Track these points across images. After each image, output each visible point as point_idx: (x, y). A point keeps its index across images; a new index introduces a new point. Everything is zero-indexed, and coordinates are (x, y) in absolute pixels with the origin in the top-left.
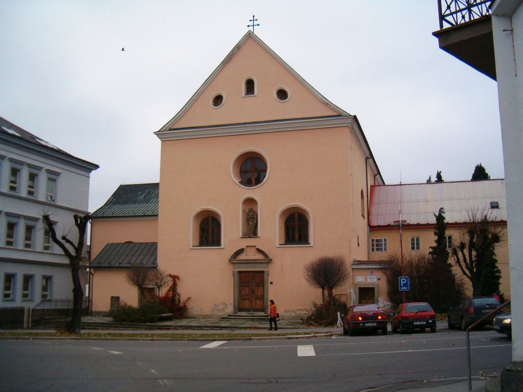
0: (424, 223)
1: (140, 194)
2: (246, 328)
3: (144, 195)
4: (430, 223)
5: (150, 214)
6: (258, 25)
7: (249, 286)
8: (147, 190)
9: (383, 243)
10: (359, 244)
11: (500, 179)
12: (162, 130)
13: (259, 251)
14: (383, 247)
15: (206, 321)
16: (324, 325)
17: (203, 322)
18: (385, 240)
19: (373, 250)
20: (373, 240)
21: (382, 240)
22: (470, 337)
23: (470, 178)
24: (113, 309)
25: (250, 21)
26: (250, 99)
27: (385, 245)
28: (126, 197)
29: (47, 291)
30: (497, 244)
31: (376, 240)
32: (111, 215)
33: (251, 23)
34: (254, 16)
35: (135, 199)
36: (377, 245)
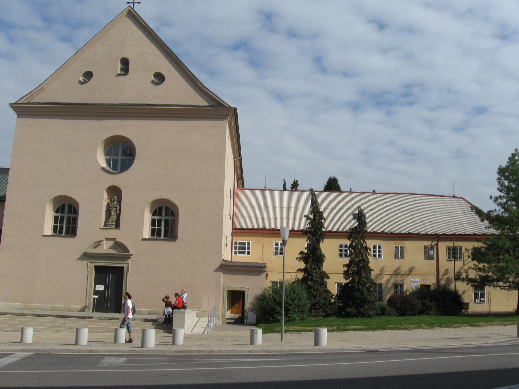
0: (471, 233)
4: (429, 233)
9: (246, 246)
11: (362, 192)
12: (19, 102)
13: (118, 245)
14: (246, 251)
18: (249, 244)
19: (236, 253)
20: (236, 243)
21: (245, 243)
23: (323, 189)
27: (248, 248)
31: (239, 243)
36: (244, 248)
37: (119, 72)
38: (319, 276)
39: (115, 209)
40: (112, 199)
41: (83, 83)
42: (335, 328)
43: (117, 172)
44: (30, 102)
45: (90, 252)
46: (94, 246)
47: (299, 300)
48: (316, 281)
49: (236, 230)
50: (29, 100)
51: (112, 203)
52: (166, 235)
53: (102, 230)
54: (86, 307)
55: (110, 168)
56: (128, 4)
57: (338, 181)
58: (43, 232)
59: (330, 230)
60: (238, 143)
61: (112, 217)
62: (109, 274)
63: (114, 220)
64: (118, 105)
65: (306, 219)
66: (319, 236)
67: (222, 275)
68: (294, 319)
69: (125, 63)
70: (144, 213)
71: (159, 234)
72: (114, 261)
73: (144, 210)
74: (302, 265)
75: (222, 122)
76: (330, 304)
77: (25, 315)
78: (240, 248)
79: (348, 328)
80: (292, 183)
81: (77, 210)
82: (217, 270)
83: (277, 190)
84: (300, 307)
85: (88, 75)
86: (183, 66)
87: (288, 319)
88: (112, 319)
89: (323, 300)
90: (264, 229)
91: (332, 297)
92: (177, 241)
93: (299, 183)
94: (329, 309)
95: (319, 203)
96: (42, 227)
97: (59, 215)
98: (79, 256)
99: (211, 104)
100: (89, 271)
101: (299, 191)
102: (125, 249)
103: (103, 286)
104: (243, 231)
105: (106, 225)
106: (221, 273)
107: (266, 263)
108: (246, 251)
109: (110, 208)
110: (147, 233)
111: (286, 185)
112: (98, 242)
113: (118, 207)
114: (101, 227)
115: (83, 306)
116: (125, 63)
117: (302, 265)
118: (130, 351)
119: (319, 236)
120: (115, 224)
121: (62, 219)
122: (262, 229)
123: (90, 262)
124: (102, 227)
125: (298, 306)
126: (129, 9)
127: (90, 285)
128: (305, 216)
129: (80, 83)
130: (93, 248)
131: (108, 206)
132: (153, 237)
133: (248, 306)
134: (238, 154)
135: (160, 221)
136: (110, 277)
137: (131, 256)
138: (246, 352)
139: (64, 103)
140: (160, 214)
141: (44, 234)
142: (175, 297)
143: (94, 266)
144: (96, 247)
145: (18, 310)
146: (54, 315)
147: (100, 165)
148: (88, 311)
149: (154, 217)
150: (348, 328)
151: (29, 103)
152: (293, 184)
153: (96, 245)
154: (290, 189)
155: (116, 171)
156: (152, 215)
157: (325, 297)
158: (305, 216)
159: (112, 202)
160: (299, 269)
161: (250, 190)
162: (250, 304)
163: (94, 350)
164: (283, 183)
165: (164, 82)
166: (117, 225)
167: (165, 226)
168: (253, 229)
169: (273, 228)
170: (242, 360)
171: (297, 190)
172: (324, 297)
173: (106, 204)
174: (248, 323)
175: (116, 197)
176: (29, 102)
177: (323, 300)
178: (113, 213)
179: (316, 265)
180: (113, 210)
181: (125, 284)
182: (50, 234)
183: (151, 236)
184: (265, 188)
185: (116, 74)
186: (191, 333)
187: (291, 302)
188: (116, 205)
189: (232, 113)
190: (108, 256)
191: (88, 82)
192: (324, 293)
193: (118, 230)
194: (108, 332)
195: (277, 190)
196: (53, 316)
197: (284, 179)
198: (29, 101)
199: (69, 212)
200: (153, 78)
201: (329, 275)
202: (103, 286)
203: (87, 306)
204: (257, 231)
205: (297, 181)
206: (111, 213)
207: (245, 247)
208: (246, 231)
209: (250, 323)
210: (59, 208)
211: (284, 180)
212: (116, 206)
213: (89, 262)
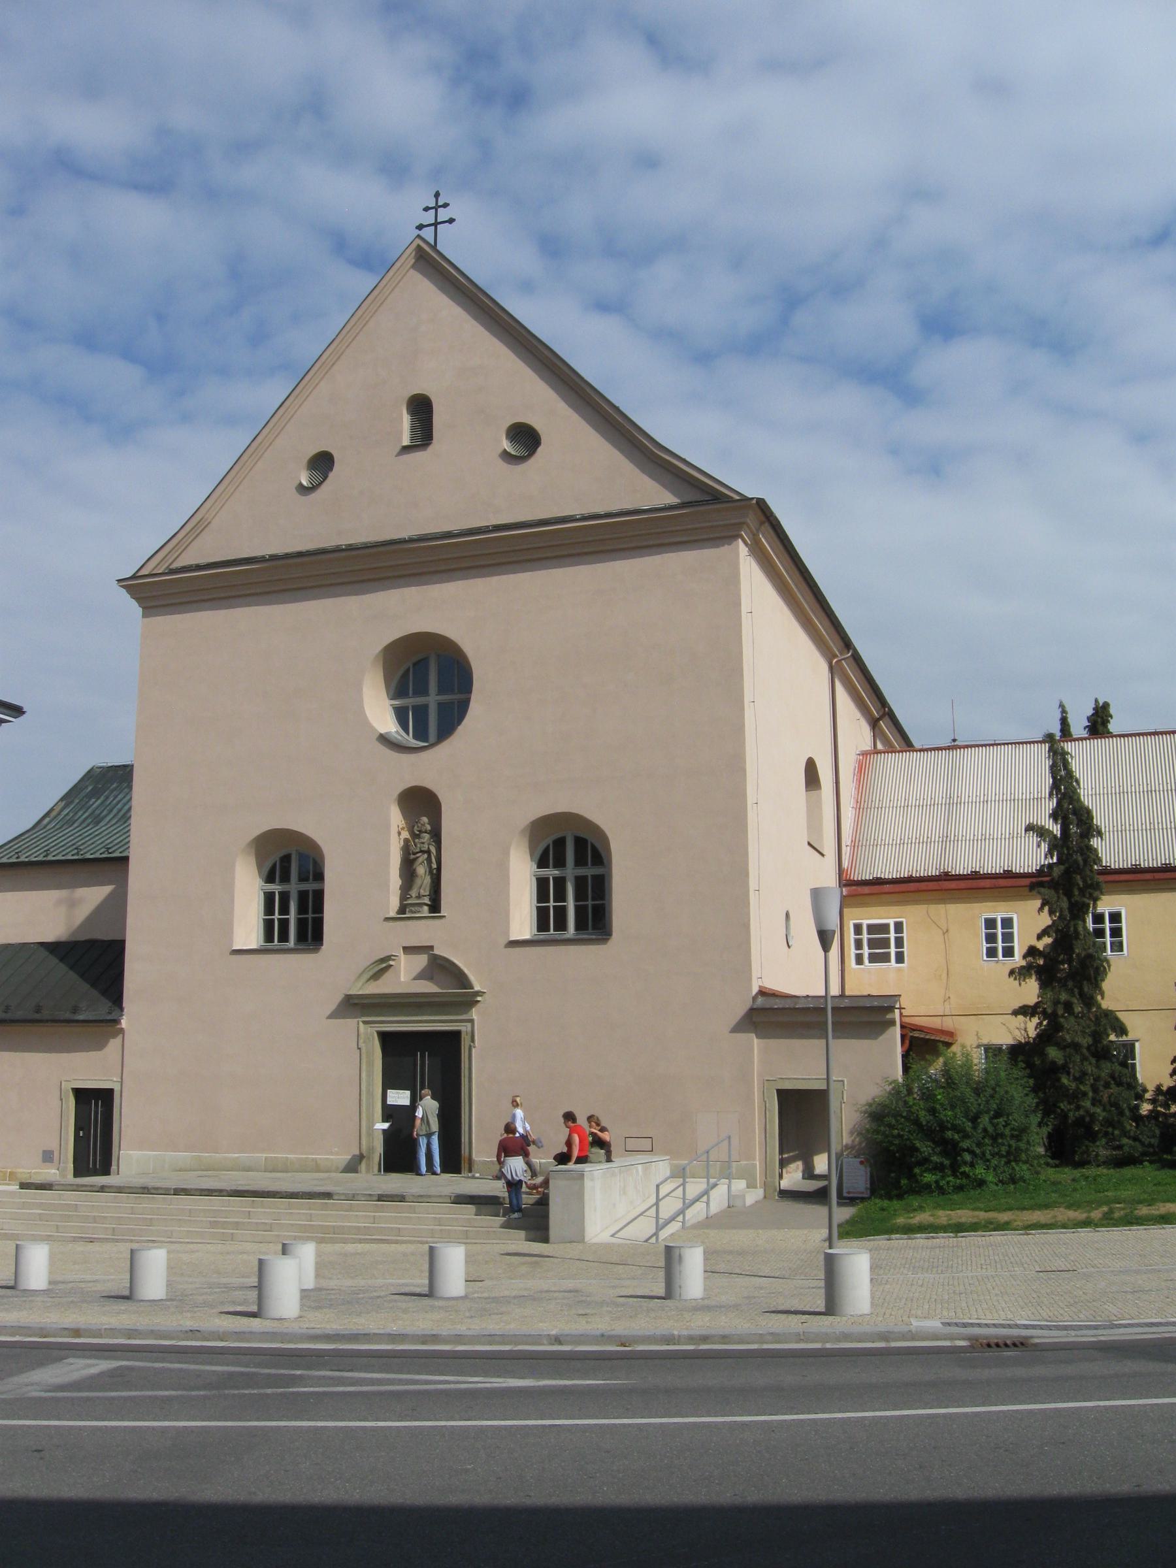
6: (451, 221)
9: (892, 935)
12: (144, 572)
13: (441, 968)
14: (893, 950)
16: (1064, 1205)
18: (899, 927)
19: (859, 960)
20: (858, 929)
21: (887, 926)
22: (427, 1282)
27: (899, 942)
29: (870, 962)
30: (870, 1101)
32: (40, 858)
33: (429, 218)
34: (437, 195)
36: (885, 943)
37: (406, 442)
38: (1089, 1027)
39: (426, 856)
40: (416, 827)
41: (311, 488)
42: (1096, 1214)
43: (426, 744)
44: (174, 566)
45: (360, 993)
46: (371, 973)
47: (998, 1114)
48: (1076, 1046)
49: (854, 888)
50: (170, 561)
51: (417, 840)
52: (581, 925)
53: (391, 924)
54: (361, 1157)
55: (407, 732)
58: (231, 941)
59: (1170, 864)
60: (826, 613)
61: (418, 881)
62: (423, 1057)
63: (426, 891)
64: (411, 540)
65: (1033, 839)
66: (1082, 891)
67: (756, 1040)
68: (981, 1183)
69: (421, 408)
70: (509, 861)
71: (561, 925)
72: (430, 1015)
73: (506, 853)
74: (1030, 991)
75: (724, 550)
76: (1138, 1118)
77: (153, 1191)
78: (872, 944)
79: (1144, 1211)
80: (1090, 712)
81: (603, 855)
82: (737, 1028)
83: (993, 745)
84: (1000, 1141)
85: (322, 463)
86: (583, 385)
87: (958, 1181)
88: (385, 1199)
89: (1108, 1107)
90: (946, 877)
91: (1140, 1097)
92: (610, 943)
93: (1112, 711)
94: (1129, 1138)
95: (1077, 782)
96: (227, 929)
97: (276, 888)
98: (332, 1006)
99: (686, 500)
100: (364, 1050)
101: (1075, 740)
102: (462, 980)
103: (408, 1093)
104: (876, 889)
105: (402, 910)
106: (753, 1035)
107: (900, 995)
108: (893, 950)
109: (412, 857)
110: (523, 924)
111: (1070, 720)
112: (383, 960)
113: (433, 850)
114: (387, 916)
115: (352, 1154)
116: (421, 408)
117: (1030, 991)
118: (186, 1332)
119: (1082, 891)
120: (429, 903)
121: (285, 897)
122: (940, 875)
123: (365, 1023)
124: (392, 914)
125: (994, 1138)
126: (419, 246)
127: (368, 1091)
128: (1030, 828)
129: (303, 490)
130: (369, 980)
131: (407, 851)
132: (543, 936)
133: (846, 1140)
134: (841, 644)
135: (560, 883)
136: (424, 1062)
137: (479, 999)
138: (545, 1342)
139: (263, 557)
140: (560, 863)
141: (235, 948)
142: (565, 1122)
143: (376, 1035)
144: (376, 976)
145: (180, 1171)
146: (228, 1189)
147: (372, 728)
148: (368, 1171)
149: (544, 872)
150: (1144, 1211)
151: (171, 570)
152: (1093, 715)
153: (377, 969)
154: (1085, 734)
155: (427, 741)
156: (538, 868)
157: (1112, 1099)
158: (1030, 828)
159: (415, 836)
160: (1021, 1008)
161: (975, 747)
162: (851, 1133)
163: (85, 1330)
164: (1059, 716)
165: (539, 449)
166: (435, 907)
167: (577, 899)
168: (910, 880)
169: (975, 872)
170: (458, 1382)
171: (1107, 734)
172: (1110, 1097)
173: (402, 843)
174: (845, 1195)
175: (425, 820)
176: (171, 567)
177: (1108, 1107)
178: (421, 870)
179: (1076, 991)
180: (420, 860)
181: (467, 1082)
182: (254, 946)
183: (538, 931)
184: (954, 740)
185: (398, 449)
186: (613, 1240)
187: (968, 1126)
188: (429, 844)
190: (412, 1000)
191: (322, 482)
192: (1113, 1086)
193: (437, 922)
194: (364, 1239)
195: (993, 745)
196: (225, 1193)
197: (1061, 702)
198: (170, 564)
199: (580, 861)
200: (506, 445)
201: (1122, 1016)
202: (408, 1093)
203: (365, 1155)
204: (923, 885)
205: (1106, 706)
206: (415, 870)
208: (887, 887)
209: (851, 1195)
210: (545, 853)
211: (1062, 706)
212: (429, 848)
213: (361, 1024)
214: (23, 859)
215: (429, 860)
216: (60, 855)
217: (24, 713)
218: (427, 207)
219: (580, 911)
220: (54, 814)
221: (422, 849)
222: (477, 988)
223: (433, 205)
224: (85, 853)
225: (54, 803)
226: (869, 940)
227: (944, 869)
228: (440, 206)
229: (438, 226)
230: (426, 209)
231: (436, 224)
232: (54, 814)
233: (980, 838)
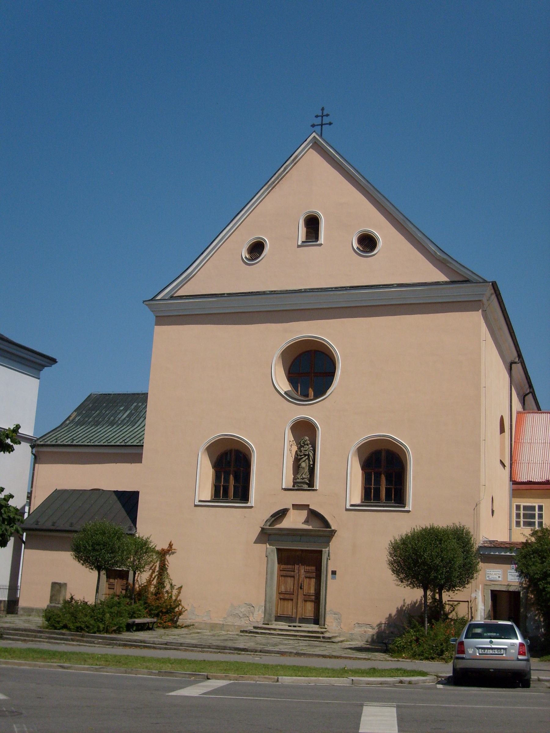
1: (121, 411)
2: (282, 653)
3: (128, 412)
5: (135, 444)
6: (330, 124)
7: (294, 577)
8: (135, 404)
9: (537, 512)
10: (493, 512)
13: (314, 515)
15: (214, 635)
17: (207, 636)
18: (541, 508)
19: (518, 524)
20: (518, 507)
21: (534, 507)
24: (53, 605)
25: (317, 116)
26: (312, 251)
28: (98, 414)
29: (523, 526)
32: (69, 443)
33: (318, 121)
34: (323, 109)
35: (112, 418)
36: (533, 516)
52: (388, 497)
56: (313, 127)
57: (435, 525)
102: (326, 524)
143: (276, 549)
189: (489, 290)
207: (535, 514)
214: (59, 442)
215: (309, 459)
216: (81, 442)
217: (57, 362)
218: (317, 115)
219: (388, 491)
220: (71, 418)
221: (305, 454)
222: (333, 528)
223: (321, 114)
224: (47, 441)
225: (71, 413)
226: (524, 514)
227: (547, 478)
228: (324, 116)
229: (323, 126)
230: (317, 116)
231: (322, 125)
232: (71, 418)
233: (541, 462)
